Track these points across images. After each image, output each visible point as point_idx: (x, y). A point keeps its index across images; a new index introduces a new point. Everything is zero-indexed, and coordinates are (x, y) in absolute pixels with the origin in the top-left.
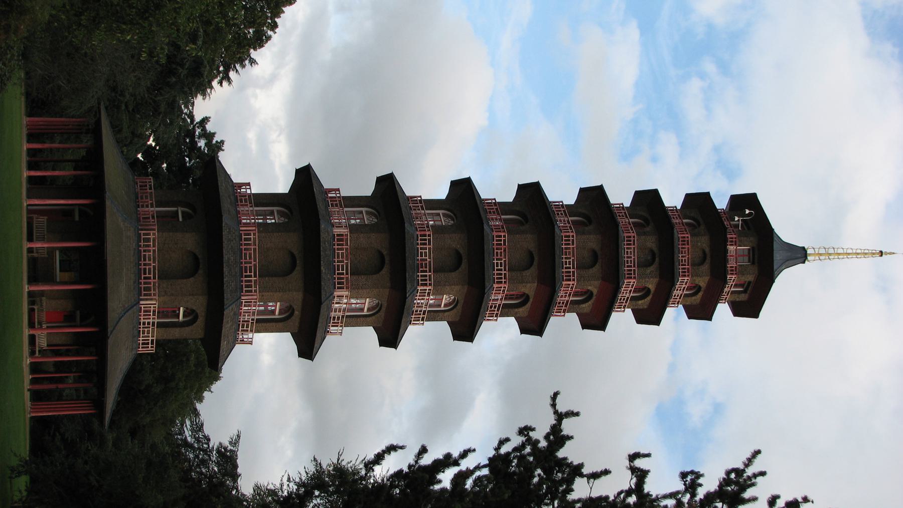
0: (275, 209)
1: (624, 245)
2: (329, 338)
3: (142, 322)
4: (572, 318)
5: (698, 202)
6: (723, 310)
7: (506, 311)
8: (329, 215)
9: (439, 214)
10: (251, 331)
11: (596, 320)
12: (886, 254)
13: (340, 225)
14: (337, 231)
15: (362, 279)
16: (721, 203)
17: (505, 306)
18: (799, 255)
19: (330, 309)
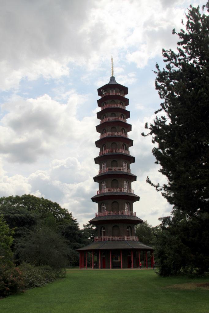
0: (102, 207)
4: (129, 133)
6: (126, 96)
7: (127, 149)
8: (104, 193)
9: (103, 185)
13: (106, 190)
14: (107, 191)
18: (113, 78)
19: (127, 193)
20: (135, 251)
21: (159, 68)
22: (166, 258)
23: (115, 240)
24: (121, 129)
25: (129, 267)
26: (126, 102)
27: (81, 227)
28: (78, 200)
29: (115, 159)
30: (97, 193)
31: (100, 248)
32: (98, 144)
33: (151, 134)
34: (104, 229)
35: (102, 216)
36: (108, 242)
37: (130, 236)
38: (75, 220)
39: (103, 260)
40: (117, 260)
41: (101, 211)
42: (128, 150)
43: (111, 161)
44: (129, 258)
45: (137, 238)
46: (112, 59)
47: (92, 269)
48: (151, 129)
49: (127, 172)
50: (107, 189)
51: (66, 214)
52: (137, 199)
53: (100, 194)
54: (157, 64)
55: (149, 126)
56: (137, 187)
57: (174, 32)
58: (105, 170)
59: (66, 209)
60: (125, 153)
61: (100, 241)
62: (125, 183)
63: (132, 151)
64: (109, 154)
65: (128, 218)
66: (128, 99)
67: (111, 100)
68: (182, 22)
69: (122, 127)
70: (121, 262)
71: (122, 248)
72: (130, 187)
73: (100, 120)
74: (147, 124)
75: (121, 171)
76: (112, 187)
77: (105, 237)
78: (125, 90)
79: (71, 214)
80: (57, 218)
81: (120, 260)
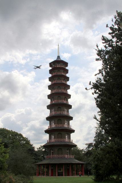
1: (57, 82)
2: (72, 128)
3: (69, 158)
4: (68, 91)
5: (50, 79)
6: (67, 68)
7: (67, 100)
8: (52, 128)
11: (70, 107)
13: (53, 126)
14: (55, 126)
16: (51, 68)
17: (67, 100)
18: (59, 57)
19: (67, 128)
20: (72, 164)
21: (98, 47)
22: (100, 169)
25: (68, 175)
26: (67, 71)
27: (36, 150)
28: (35, 131)
29: (60, 107)
31: (50, 163)
32: (49, 107)
33: (92, 88)
34: (52, 150)
36: (55, 159)
38: (32, 144)
39: (64, 169)
40: (61, 170)
44: (68, 169)
47: (45, 177)
48: (93, 85)
51: (26, 141)
52: (73, 131)
54: (97, 45)
55: (92, 84)
57: (107, 26)
59: (26, 138)
61: (50, 158)
62: (66, 121)
65: (68, 144)
68: (112, 20)
70: (64, 172)
71: (64, 163)
72: (69, 124)
74: (90, 82)
76: (58, 124)
77: (53, 156)
78: (66, 64)
79: (29, 141)
80: (21, 144)
81: (63, 170)
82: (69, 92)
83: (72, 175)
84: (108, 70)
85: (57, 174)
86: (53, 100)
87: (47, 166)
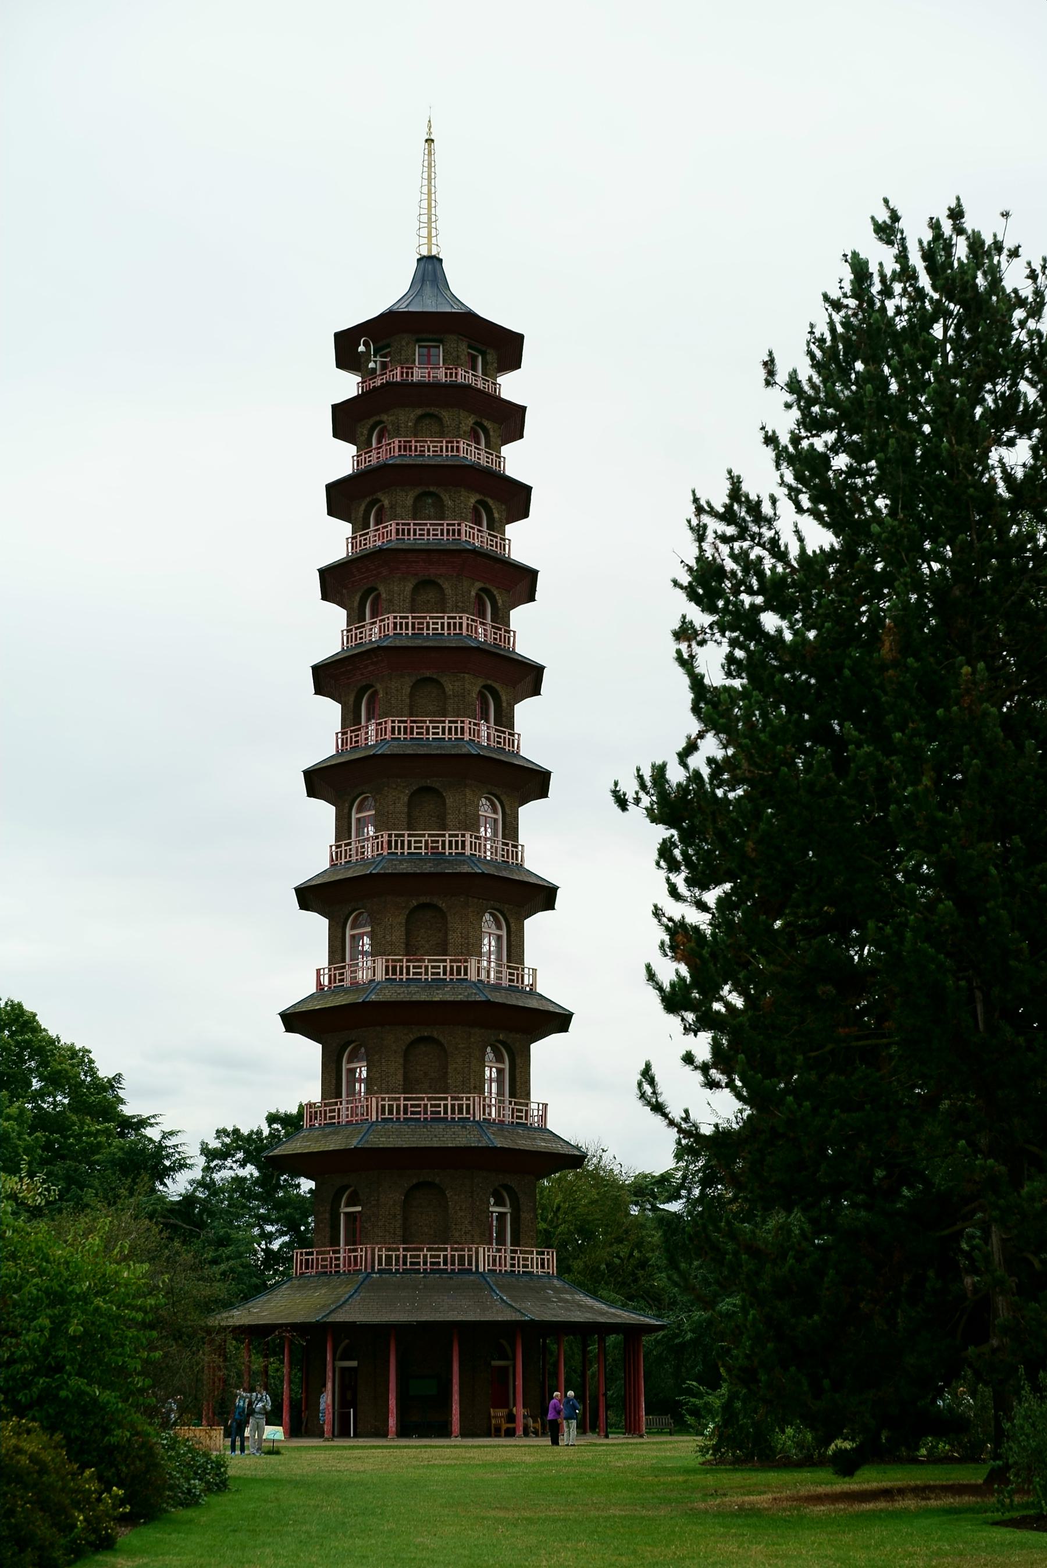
0: (345, 1067)
1: (411, 458)
3: (508, 1278)
4: (513, 530)
7: (502, 620)
10: (527, 1105)
12: (430, 134)
13: (368, 970)
14: (380, 976)
15: (454, 938)
18: (430, 268)
19: (497, 987)
23: (422, 1267)
24: (473, 501)
28: (208, 1032)
29: (433, 410)
30: (319, 983)
31: (340, 1317)
35: (344, 1120)
37: (509, 1247)
41: (339, 1095)
42: (512, 727)
43: (409, 586)
45: (551, 1257)
46: (429, 141)
49: (499, 859)
50: (380, 963)
53: (334, 991)
56: (543, 841)
58: (371, 842)
60: (490, 641)
62: (485, 810)
63: (536, 730)
64: (396, 751)
66: (523, 409)
67: (419, 412)
69: (479, 585)
73: (352, 449)
75: (468, 852)
82: (529, 631)
83: (477, 1427)
84: (950, 359)
85: (392, 1422)
86: (379, 441)
87: (308, 1342)
